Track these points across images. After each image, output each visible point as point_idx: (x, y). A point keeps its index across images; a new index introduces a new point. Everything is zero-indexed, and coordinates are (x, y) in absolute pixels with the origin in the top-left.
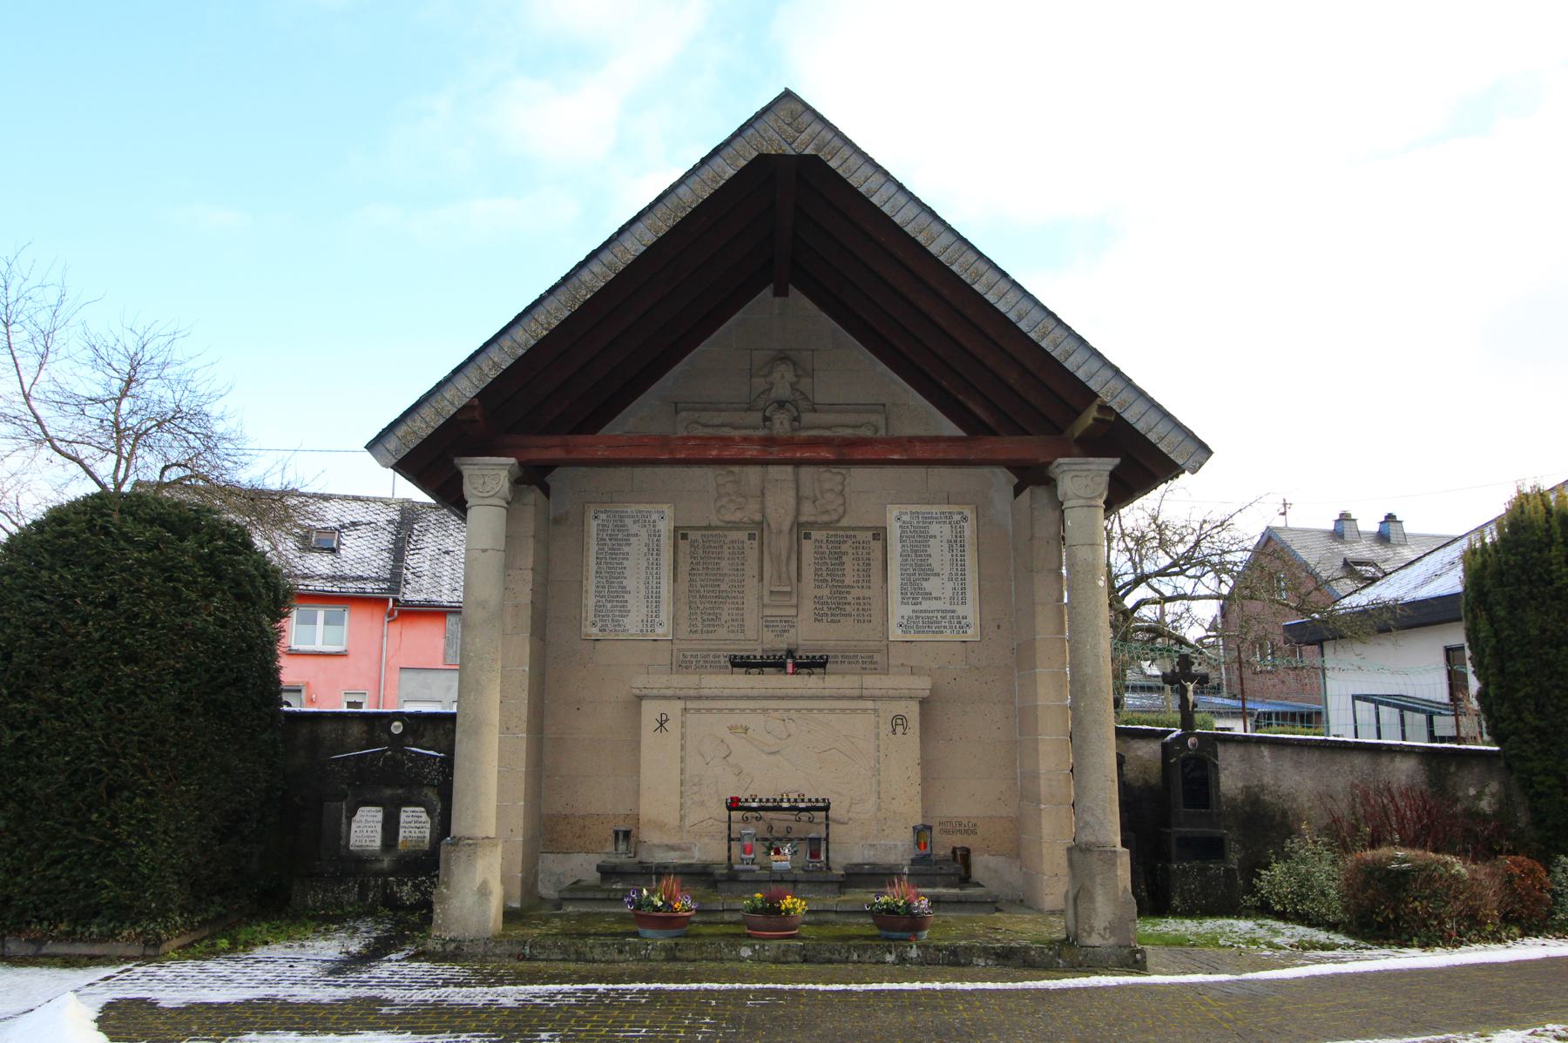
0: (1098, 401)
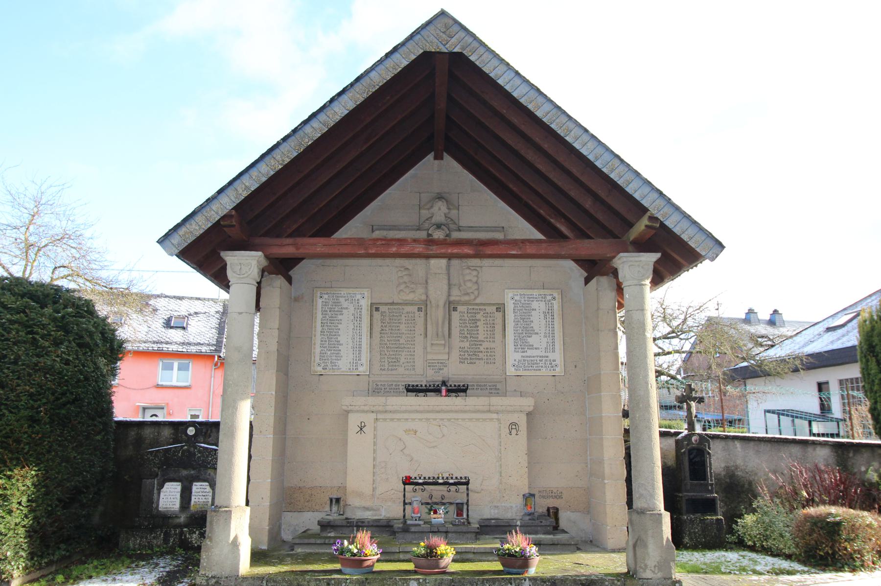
0: (648, 214)
